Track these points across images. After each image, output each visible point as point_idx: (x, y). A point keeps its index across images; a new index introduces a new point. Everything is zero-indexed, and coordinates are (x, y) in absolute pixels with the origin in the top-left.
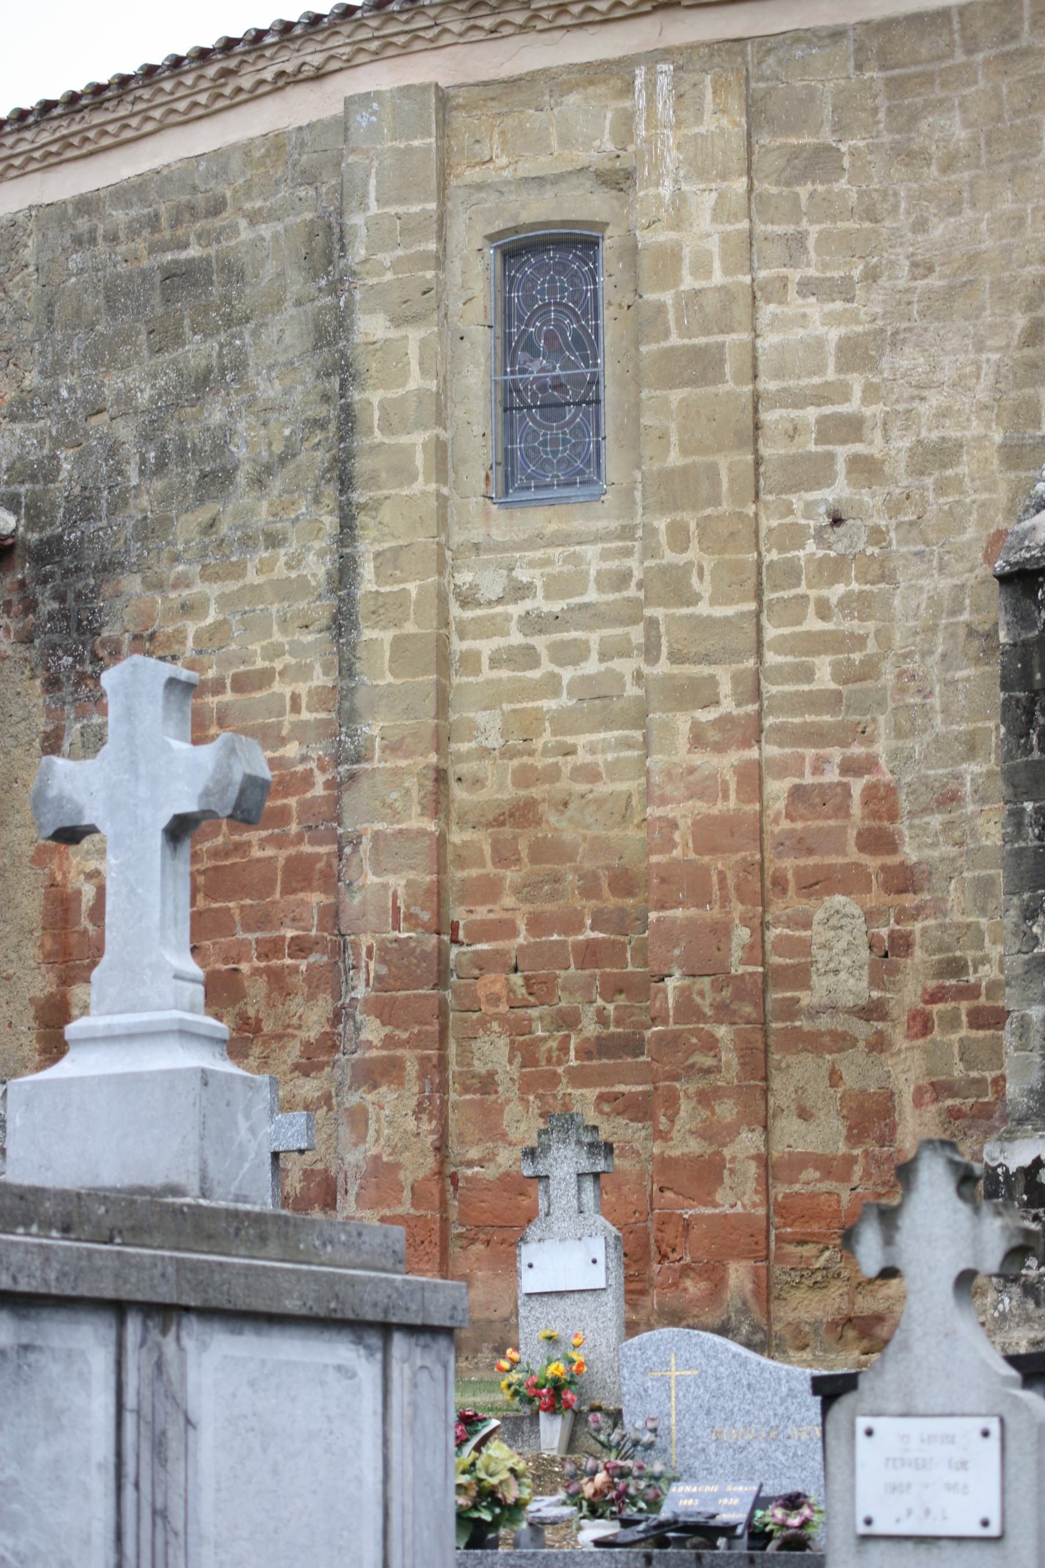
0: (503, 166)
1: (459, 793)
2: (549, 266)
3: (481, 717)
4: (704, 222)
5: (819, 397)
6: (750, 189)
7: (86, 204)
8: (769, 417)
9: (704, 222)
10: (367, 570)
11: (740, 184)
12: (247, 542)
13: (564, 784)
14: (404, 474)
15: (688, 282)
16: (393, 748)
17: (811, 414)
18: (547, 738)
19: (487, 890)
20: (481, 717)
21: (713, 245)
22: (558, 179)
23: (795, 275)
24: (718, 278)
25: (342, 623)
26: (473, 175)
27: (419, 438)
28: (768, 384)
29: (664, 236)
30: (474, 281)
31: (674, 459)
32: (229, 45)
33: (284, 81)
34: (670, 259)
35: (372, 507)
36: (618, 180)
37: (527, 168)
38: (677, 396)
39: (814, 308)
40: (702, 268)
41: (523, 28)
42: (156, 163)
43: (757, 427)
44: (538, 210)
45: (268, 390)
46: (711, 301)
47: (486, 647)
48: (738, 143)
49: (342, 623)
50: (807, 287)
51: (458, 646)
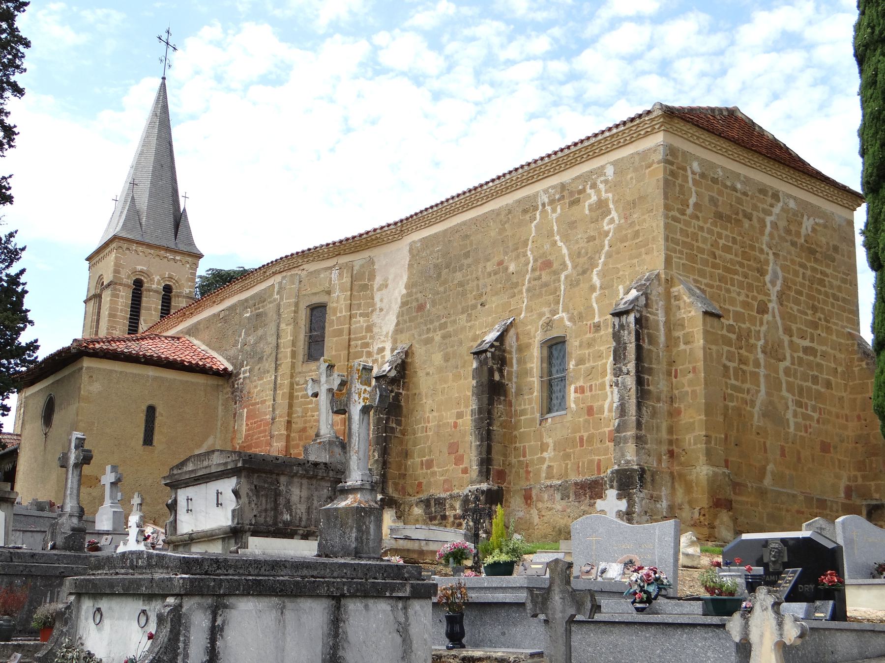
0: (309, 291)
1: (293, 425)
2: (318, 312)
3: (298, 409)
4: (342, 302)
5: (361, 339)
6: (351, 295)
7: (246, 300)
8: (352, 343)
9: (342, 302)
10: (279, 378)
11: (349, 293)
12: (264, 373)
13: (312, 423)
14: (286, 357)
15: (339, 315)
16: (280, 417)
17: (360, 342)
18: (310, 413)
19: (297, 446)
20: (298, 409)
21: (343, 306)
22: (318, 293)
23: (358, 312)
24: (344, 313)
25: (275, 389)
26: (304, 293)
27: (289, 350)
28: (352, 336)
29: (335, 305)
30: (303, 315)
31: (334, 353)
32: (264, 266)
33: (274, 273)
34: (335, 310)
35: (280, 365)
36: (329, 293)
37: (314, 291)
38: (335, 339)
39: (362, 319)
40: (341, 312)
41: (313, 261)
42: (452, 225)
43: (349, 345)
44: (316, 300)
45: (269, 340)
46: (342, 319)
47: (300, 394)
48: (349, 284)
49: (275, 389)
50: (361, 315)
51: (296, 394)
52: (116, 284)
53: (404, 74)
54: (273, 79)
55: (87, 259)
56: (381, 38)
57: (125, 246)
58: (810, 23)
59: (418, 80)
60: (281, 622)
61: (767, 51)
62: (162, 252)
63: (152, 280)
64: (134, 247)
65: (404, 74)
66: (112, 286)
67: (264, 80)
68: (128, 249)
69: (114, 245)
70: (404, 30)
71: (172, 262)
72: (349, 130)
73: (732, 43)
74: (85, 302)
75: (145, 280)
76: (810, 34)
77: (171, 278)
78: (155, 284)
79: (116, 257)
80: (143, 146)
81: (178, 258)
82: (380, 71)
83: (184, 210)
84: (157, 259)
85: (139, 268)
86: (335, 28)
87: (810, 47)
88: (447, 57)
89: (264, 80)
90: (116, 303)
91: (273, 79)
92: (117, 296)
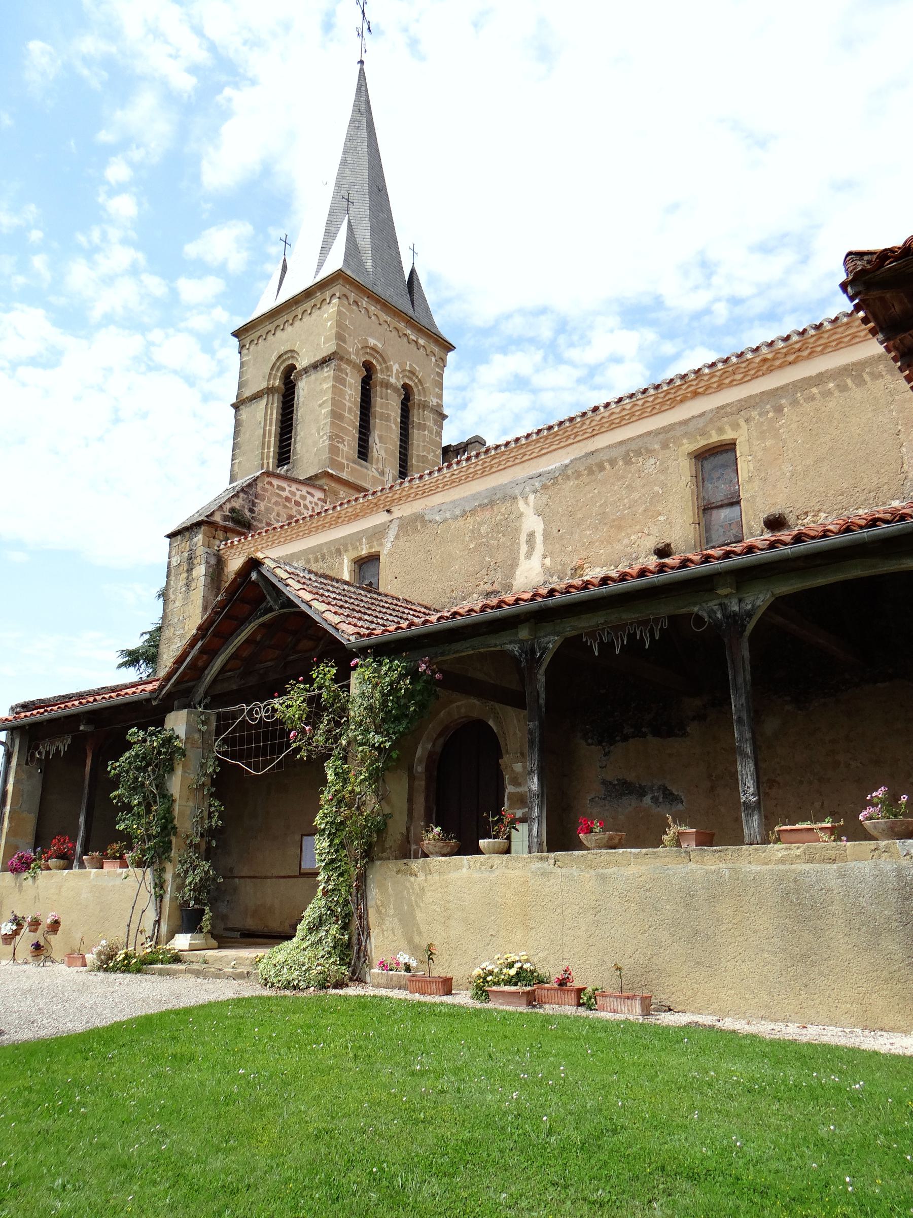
52: (341, 359)
53: (175, 372)
54: (49, 360)
55: (236, 334)
56: (156, 335)
57: (352, 296)
58: (537, 371)
59: (190, 381)
60: (16, 879)
61: (502, 391)
62: (402, 325)
63: (388, 369)
64: (364, 302)
65: (175, 372)
66: (333, 364)
67: (33, 362)
68: (356, 302)
69: (337, 289)
70: (179, 331)
71: (413, 346)
72: (117, 421)
73: (473, 380)
74: (236, 407)
75: (378, 368)
76: (538, 380)
77: (412, 372)
78: (393, 374)
79: (339, 312)
80: (345, 152)
81: (421, 342)
82: (154, 368)
83: (413, 272)
84: (395, 333)
85: (372, 342)
86: (108, 320)
87: (535, 391)
88: (220, 362)
89: (33, 362)
90: (342, 394)
91: (49, 360)
92: (343, 382)
